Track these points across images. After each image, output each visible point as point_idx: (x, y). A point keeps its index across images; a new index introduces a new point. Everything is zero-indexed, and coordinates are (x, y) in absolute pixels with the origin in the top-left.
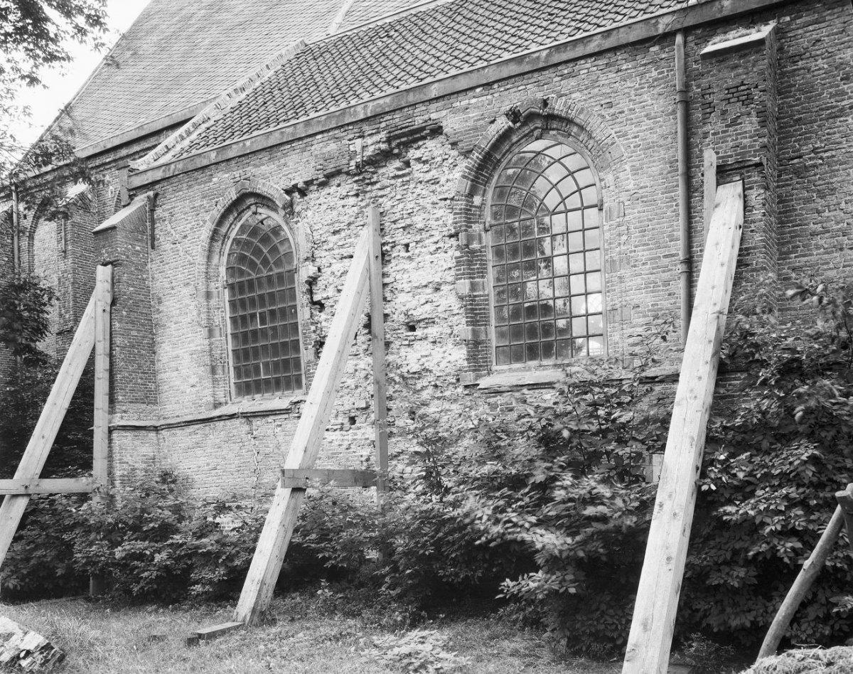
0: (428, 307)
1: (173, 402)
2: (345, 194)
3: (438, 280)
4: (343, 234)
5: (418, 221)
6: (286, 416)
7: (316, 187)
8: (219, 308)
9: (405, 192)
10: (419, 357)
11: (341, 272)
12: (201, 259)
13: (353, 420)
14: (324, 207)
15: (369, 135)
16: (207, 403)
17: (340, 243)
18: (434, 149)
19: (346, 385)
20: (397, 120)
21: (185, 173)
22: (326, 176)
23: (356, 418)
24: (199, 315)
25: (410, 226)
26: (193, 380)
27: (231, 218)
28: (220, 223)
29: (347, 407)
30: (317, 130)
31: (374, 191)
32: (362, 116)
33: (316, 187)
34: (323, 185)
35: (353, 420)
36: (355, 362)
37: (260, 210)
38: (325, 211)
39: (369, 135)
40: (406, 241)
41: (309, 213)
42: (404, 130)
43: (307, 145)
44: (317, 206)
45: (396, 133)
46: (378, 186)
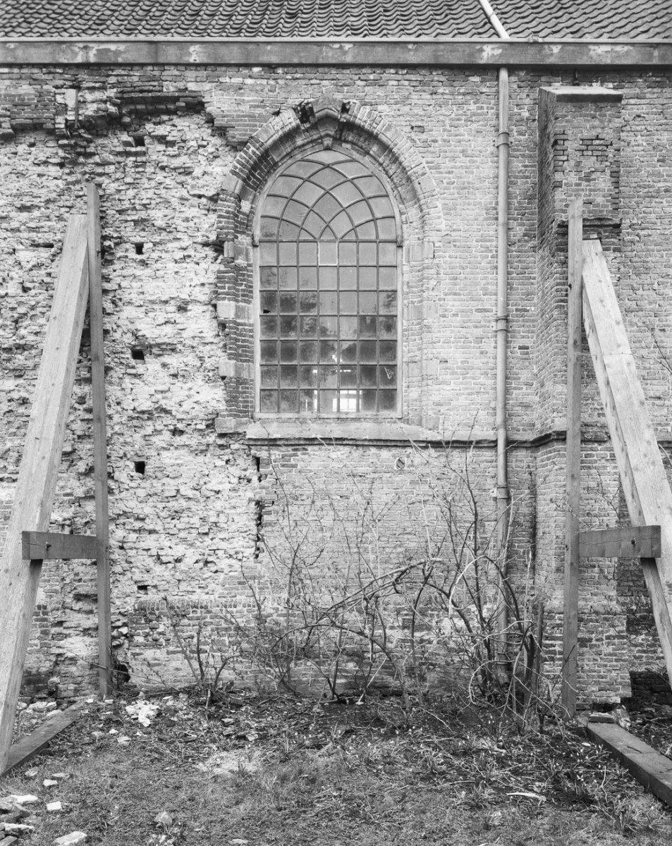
0: (168, 329)
2: (44, 159)
3: (184, 296)
4: (36, 213)
5: (158, 216)
9: (138, 176)
11: (32, 263)
15: (88, 88)
17: (32, 225)
18: (186, 129)
20: (136, 79)
22: (13, 127)
25: (143, 220)
39: (88, 88)
40: (138, 240)
42: (145, 94)
46: (97, 159)
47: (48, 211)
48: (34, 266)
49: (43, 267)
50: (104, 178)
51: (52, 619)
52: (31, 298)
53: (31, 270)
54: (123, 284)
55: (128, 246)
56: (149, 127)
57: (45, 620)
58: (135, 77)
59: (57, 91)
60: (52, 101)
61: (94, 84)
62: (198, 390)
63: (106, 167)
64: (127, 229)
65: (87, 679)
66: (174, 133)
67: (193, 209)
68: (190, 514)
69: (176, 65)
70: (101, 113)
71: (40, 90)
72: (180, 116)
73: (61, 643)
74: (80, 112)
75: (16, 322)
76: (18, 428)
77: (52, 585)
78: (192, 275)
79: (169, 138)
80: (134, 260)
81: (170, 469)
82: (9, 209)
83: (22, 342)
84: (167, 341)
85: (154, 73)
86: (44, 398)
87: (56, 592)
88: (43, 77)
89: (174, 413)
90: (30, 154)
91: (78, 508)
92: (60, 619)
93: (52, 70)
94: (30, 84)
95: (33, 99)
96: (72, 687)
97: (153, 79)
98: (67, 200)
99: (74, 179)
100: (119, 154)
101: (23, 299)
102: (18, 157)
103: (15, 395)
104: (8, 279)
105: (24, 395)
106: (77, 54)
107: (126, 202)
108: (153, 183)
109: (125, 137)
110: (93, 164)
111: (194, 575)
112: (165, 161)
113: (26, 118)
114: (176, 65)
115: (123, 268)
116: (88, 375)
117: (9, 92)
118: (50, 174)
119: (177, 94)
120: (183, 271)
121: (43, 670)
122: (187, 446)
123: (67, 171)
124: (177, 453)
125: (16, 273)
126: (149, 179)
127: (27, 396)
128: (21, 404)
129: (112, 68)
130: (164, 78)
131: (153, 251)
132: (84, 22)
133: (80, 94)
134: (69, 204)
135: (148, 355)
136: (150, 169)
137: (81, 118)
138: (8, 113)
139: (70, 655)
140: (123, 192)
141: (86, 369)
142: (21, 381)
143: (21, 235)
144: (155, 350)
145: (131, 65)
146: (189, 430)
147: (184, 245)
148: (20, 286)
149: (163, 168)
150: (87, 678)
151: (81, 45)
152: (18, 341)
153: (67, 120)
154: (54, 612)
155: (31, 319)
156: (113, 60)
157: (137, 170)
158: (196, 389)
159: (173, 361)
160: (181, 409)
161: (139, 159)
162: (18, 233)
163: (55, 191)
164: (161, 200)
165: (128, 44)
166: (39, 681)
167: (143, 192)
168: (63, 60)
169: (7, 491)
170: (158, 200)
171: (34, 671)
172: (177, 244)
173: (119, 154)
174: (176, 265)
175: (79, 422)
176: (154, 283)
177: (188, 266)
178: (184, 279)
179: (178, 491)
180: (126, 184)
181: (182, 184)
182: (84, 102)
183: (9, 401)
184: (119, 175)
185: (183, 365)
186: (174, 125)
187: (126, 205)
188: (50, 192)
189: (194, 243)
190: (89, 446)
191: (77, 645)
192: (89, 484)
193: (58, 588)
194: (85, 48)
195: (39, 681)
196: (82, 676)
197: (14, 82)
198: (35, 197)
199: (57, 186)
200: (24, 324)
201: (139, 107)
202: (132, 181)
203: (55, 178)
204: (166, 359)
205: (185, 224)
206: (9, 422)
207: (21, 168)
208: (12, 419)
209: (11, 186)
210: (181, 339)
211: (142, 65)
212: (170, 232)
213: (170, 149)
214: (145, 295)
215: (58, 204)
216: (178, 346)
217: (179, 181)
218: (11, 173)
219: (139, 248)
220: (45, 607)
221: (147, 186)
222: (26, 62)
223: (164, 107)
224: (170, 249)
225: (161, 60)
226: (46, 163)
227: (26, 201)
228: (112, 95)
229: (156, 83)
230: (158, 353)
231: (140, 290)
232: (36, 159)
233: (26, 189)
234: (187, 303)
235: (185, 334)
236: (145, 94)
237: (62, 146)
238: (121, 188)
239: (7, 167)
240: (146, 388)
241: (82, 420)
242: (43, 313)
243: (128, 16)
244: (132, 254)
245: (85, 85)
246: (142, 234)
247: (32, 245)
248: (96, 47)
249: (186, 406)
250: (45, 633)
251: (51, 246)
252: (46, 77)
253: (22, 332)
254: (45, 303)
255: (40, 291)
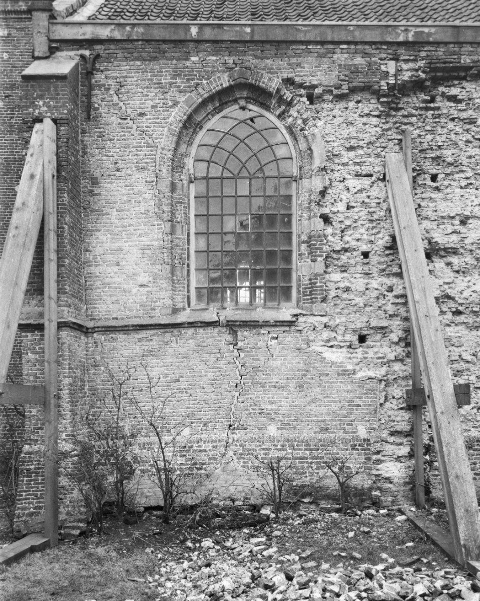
0: (454, 238)
1: (108, 302)
2: (368, 112)
3: (467, 213)
4: (360, 152)
5: (448, 154)
6: (288, 329)
7: (331, 97)
8: (182, 203)
9: (435, 125)
10: (442, 284)
11: (358, 188)
12: (167, 142)
13: (362, 339)
14: (339, 120)
15: (404, 60)
16: (164, 307)
17: (357, 160)
18: (473, 90)
19: (353, 302)
20: (441, 53)
21: (147, 41)
22: (349, 89)
23: (367, 337)
24: (159, 206)
25: (438, 157)
26: (144, 278)
27: (210, 107)
28: (196, 110)
29: (359, 325)
30: (343, 39)
31: (399, 116)
32: (401, 39)
33: (331, 97)
34: (341, 97)
35: (362, 339)
36: (366, 281)
37: (251, 107)
38: (339, 125)
39: (404, 60)
40: (434, 172)
41: (320, 123)
42: (447, 65)
43: (328, 51)
44: (331, 117)
45: (438, 65)
46: (403, 112)
47: (369, 150)
48: (358, 191)
49: (364, 192)
50: (408, 126)
51: (373, 449)
52: (355, 214)
53: (356, 193)
54: (423, 204)
55: (427, 176)
56: (441, 89)
57: (369, 450)
58: (441, 52)
59: (382, 62)
60: (378, 70)
61: (409, 57)
62: (475, 282)
63: (410, 118)
64: (426, 164)
65: (401, 493)
66: (463, 93)
67: (474, 149)
68: (469, 373)
69: (471, 43)
70: (414, 78)
71: (369, 62)
72: (468, 81)
73: (380, 466)
74: (399, 78)
75: (343, 232)
76: (342, 309)
77: (371, 424)
78: (473, 198)
79: (459, 97)
80: (431, 187)
81: (454, 340)
82: (341, 149)
83: (347, 246)
84: (453, 246)
85: (455, 49)
86: (420, 286)
87: (374, 429)
88: (373, 52)
89: (456, 299)
90: (357, 108)
91: (388, 368)
92: (379, 449)
93: (380, 47)
94: (362, 57)
95: (365, 68)
96: (390, 499)
97: (454, 53)
98: (383, 142)
99: (388, 127)
100: (421, 109)
101: (349, 215)
102: (348, 111)
103: (341, 285)
104: (338, 200)
105: (348, 285)
106: (399, 35)
107: (425, 144)
108: (445, 131)
109: (423, 96)
110: (400, 116)
111: (470, 418)
112: (455, 114)
113: (360, 82)
114: (471, 43)
115: (422, 193)
116: (399, 271)
117: (347, 63)
118: (371, 123)
119: (471, 65)
120: (467, 195)
121: (366, 486)
122: (465, 323)
123: (384, 121)
124: (457, 328)
125: (345, 196)
126: (442, 127)
127: (350, 286)
128: (344, 291)
129: (423, 45)
130: (462, 53)
131: (444, 180)
132: (109, 10)
133: (398, 64)
134: (384, 145)
135: (434, 256)
136: (443, 120)
137: (399, 82)
138: (347, 78)
139: (387, 475)
140: (422, 137)
141: (398, 266)
142: (345, 274)
143: (349, 167)
144: (442, 253)
145: (437, 44)
146: (467, 311)
147: (468, 175)
148: (346, 205)
149: (453, 120)
150: (401, 492)
151: (403, 28)
152: (343, 246)
153: (388, 84)
154: (375, 444)
155: (353, 229)
156: (426, 39)
157: (434, 120)
158: (473, 281)
159: (455, 260)
160: (463, 296)
161: (436, 112)
162: (347, 167)
163: (375, 136)
164: (452, 143)
165: (437, 28)
166: (363, 494)
167: (438, 137)
168: (389, 39)
169: (336, 355)
170: (450, 143)
171: (359, 487)
172: (463, 175)
173: (421, 109)
174: (462, 190)
175: (390, 305)
176: (445, 204)
177: (471, 191)
178: (467, 201)
179: (460, 356)
180: (426, 131)
181: (467, 131)
182: (401, 70)
183: (336, 289)
184: (420, 124)
185: (464, 264)
186: (463, 88)
187: (425, 146)
188: (371, 136)
189: (475, 174)
190: (398, 323)
191: (391, 469)
192: (398, 350)
193: (376, 426)
194: (406, 30)
195: (363, 494)
196: (398, 491)
197: (351, 56)
198: (361, 140)
199: (377, 132)
200: (349, 233)
201: (438, 74)
202: (430, 129)
203: (376, 126)
204: (450, 259)
205: (468, 160)
206: (335, 305)
207: (351, 119)
208: (338, 302)
209: (343, 132)
210: (464, 245)
211: (446, 43)
212: (457, 166)
213: (459, 105)
214: (438, 212)
215: (376, 145)
216: (460, 250)
217: (465, 129)
218: (343, 123)
219: (434, 178)
220: (369, 440)
221: (440, 132)
222: (362, 40)
223: (456, 74)
224: (457, 179)
225: (462, 40)
226: (368, 115)
227: (353, 143)
228: (422, 65)
229: (456, 57)
230: (443, 254)
231: (435, 209)
232: (362, 112)
233: (353, 134)
234: (468, 218)
235: (466, 241)
236: (447, 65)
237: (382, 103)
238: (421, 134)
239: (341, 118)
240: (437, 280)
241: (392, 304)
242: (363, 225)
243: (126, 5)
244: (429, 182)
245: (402, 58)
246: (437, 167)
247: (356, 175)
248: (414, 30)
249: (466, 294)
250: (368, 459)
251: (370, 176)
252: (374, 52)
253: (347, 238)
254: (365, 218)
255: (361, 209)
